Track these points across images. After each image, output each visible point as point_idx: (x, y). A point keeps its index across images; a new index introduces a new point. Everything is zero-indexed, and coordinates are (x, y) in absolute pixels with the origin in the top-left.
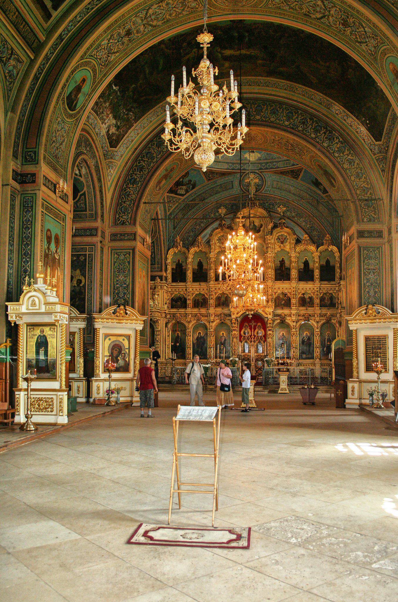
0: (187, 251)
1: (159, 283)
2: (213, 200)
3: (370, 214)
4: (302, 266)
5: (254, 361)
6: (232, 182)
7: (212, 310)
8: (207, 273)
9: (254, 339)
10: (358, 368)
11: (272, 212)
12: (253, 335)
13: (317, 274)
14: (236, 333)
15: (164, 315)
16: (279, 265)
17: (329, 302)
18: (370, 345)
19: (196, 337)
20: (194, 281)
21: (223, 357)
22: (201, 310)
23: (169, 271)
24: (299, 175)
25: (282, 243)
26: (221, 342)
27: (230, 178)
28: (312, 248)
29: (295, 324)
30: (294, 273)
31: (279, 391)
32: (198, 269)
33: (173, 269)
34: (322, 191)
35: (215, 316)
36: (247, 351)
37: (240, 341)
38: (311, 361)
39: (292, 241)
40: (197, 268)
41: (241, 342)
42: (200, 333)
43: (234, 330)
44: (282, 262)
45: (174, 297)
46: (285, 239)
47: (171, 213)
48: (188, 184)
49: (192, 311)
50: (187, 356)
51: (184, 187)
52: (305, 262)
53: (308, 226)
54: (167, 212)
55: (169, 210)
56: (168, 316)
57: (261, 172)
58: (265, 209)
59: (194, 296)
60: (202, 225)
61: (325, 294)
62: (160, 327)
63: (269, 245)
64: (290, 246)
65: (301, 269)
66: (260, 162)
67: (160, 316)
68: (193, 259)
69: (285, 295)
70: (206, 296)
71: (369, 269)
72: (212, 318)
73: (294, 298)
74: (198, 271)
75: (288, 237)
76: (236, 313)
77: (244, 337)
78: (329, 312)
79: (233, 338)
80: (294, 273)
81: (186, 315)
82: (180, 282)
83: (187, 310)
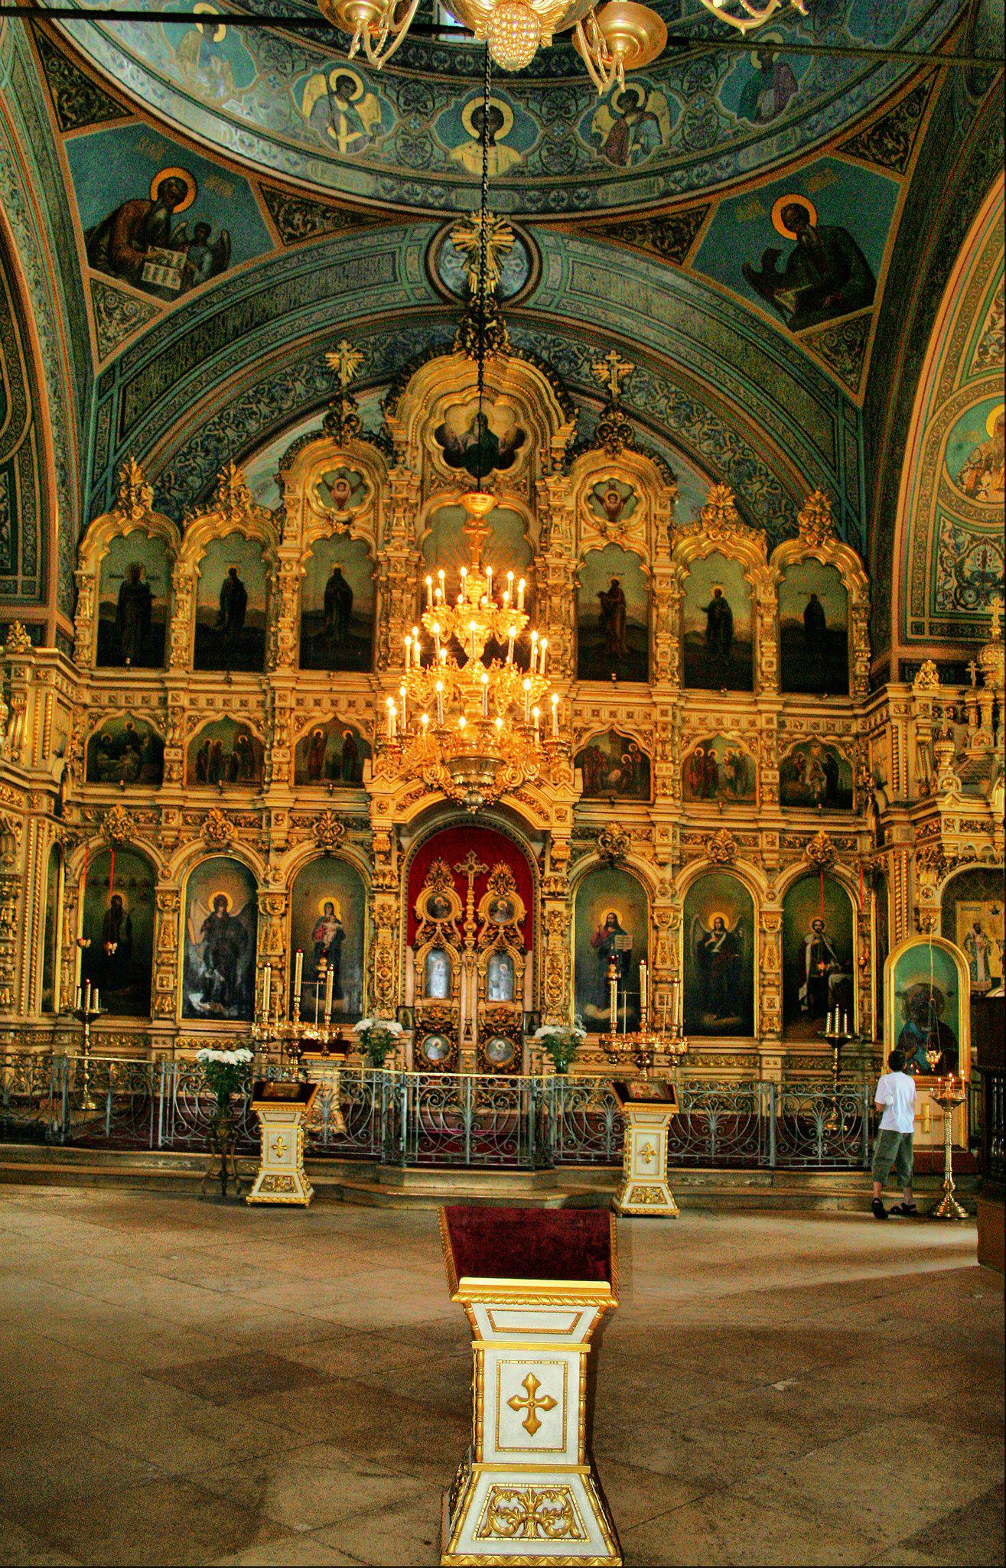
0: (173, 531)
1: (27, 652)
2: (303, 323)
5: (475, 1035)
6: (393, 254)
7: (279, 796)
8: (263, 632)
9: (476, 934)
12: (470, 917)
14: (391, 903)
15: (45, 805)
16: (597, 612)
17: (819, 787)
19: (200, 917)
21: (322, 1014)
22: (228, 796)
23: (89, 609)
24: (691, 242)
25: (613, 515)
26: (320, 945)
27: (388, 240)
28: (750, 545)
29: (667, 874)
30: (666, 650)
32: (221, 614)
33: (104, 607)
34: (789, 316)
35: (295, 823)
36: (438, 990)
37: (412, 942)
38: (739, 1043)
40: (216, 605)
41: (416, 949)
42: (221, 901)
43: (384, 889)
44: (613, 598)
48: (194, 243)
50: (156, 1003)
51: (176, 255)
52: (713, 606)
53: (726, 457)
54: (95, 361)
55: (103, 353)
56: (74, 817)
57: (521, 223)
59: (198, 729)
60: (253, 426)
61: (805, 746)
63: (556, 520)
65: (697, 634)
66: (520, 181)
67: (24, 808)
69: (624, 742)
70: (255, 732)
72: (278, 835)
73: (664, 757)
74: (221, 622)
75: (639, 493)
76: (392, 806)
77: (428, 924)
78: (822, 827)
79: (376, 927)
80: (666, 650)
83: (162, 792)
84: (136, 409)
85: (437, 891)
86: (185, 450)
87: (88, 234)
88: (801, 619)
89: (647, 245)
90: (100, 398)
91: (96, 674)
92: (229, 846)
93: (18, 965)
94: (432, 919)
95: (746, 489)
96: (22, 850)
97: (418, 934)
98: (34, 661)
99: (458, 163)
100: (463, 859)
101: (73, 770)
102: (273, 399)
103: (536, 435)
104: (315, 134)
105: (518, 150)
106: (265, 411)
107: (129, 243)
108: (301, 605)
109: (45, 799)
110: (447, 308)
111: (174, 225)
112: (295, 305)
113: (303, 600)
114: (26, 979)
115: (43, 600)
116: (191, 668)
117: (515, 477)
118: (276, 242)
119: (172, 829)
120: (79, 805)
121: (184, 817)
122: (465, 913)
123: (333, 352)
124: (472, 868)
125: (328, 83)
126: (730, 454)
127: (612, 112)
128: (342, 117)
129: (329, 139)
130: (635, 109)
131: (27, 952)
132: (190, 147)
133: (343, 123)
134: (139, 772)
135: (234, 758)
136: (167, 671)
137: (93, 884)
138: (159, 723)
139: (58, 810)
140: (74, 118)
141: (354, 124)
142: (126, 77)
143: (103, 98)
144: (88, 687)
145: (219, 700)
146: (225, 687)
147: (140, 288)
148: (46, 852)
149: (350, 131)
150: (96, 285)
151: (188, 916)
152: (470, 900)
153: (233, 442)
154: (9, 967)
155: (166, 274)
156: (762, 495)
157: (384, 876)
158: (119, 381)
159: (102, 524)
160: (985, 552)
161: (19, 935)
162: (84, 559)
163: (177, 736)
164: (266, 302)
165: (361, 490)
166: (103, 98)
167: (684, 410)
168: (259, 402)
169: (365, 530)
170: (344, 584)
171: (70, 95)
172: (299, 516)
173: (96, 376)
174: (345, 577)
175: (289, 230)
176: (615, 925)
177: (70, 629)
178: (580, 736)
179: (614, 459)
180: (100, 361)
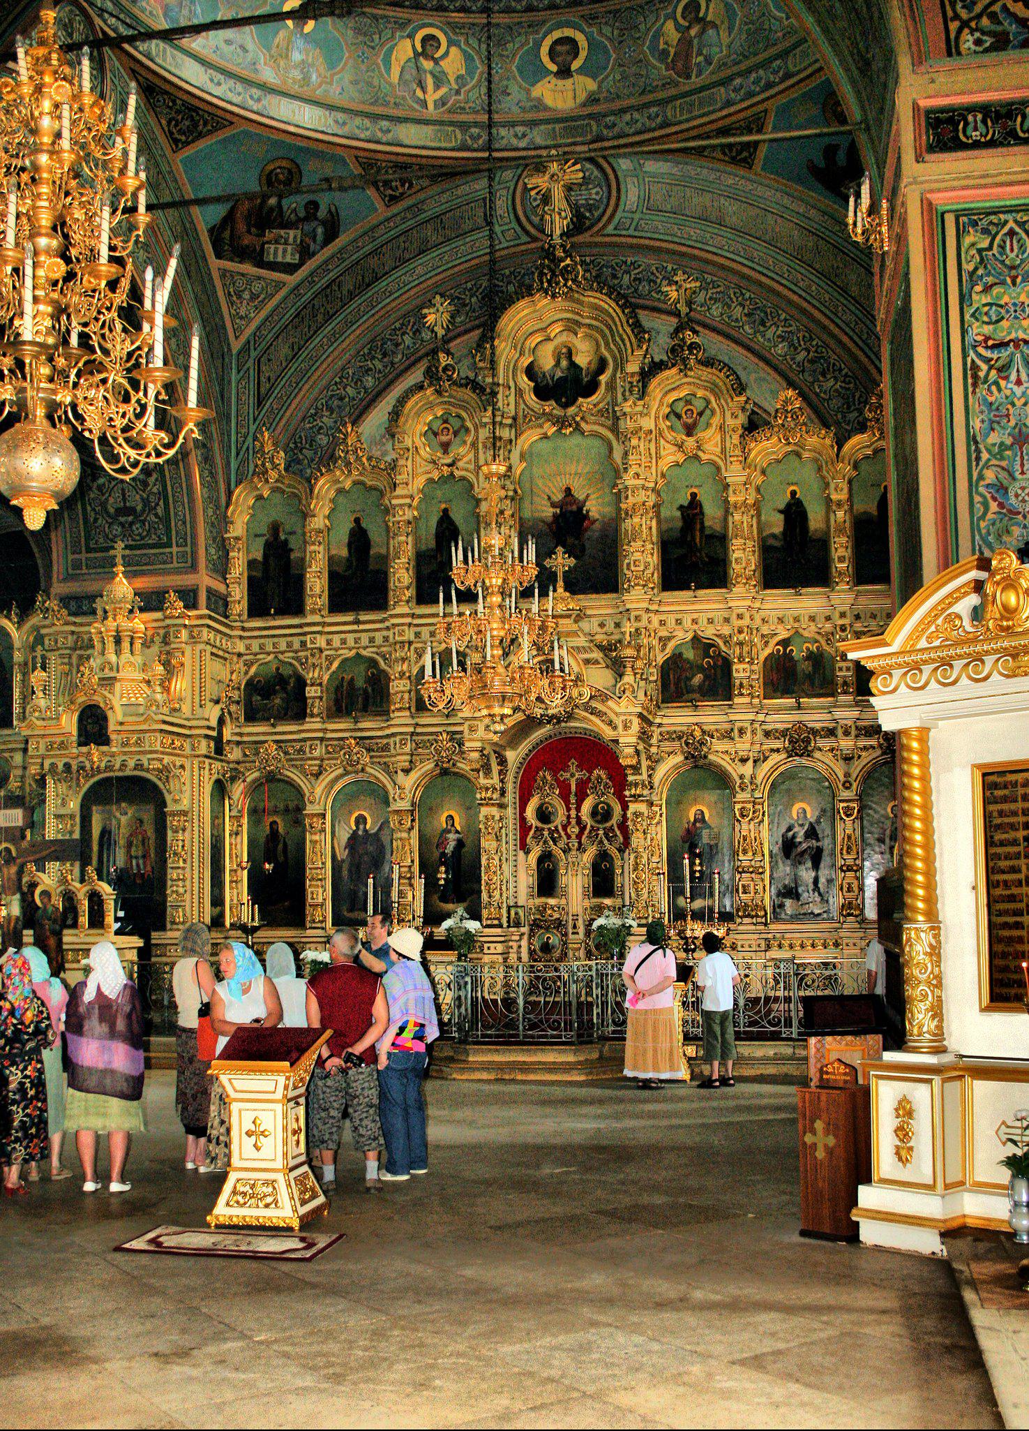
0: (301, 489)
4: (776, 524)
9: (579, 836)
10: (938, 982)
11: (645, 308)
12: (573, 821)
13: (841, 552)
15: (204, 747)
16: (679, 524)
18: (1013, 827)
19: (344, 835)
20: (336, 605)
23: (238, 569)
25: (690, 430)
32: (348, 560)
33: (251, 564)
39: (730, 422)
40: (344, 552)
41: (527, 853)
42: (361, 820)
44: (692, 510)
45: (256, 675)
49: (325, 730)
51: (292, 233)
52: (789, 506)
55: (238, 332)
56: (235, 754)
58: (614, 292)
59: (335, 665)
60: (369, 381)
62: (187, 794)
64: (723, 441)
65: (774, 536)
67: (188, 751)
68: (328, 517)
71: (1003, 345)
74: (349, 567)
82: (276, 613)
84: (269, 379)
85: (543, 797)
86: (312, 411)
87: (211, 231)
91: (247, 625)
92: (363, 770)
93: (188, 887)
94: (540, 825)
97: (528, 840)
98: (187, 622)
99: (539, 100)
100: (565, 768)
101: (230, 713)
102: (385, 355)
103: (614, 358)
104: (404, 98)
105: (594, 77)
106: (379, 366)
107: (249, 232)
108: (415, 544)
109: (204, 742)
110: (533, 245)
111: (285, 208)
113: (417, 540)
114: (196, 900)
115: (194, 568)
116: (326, 612)
117: (598, 403)
118: (379, 205)
119: (315, 759)
120: (238, 743)
121: (327, 746)
122: (569, 817)
123: (428, 307)
124: (573, 774)
125: (413, 46)
126: (804, 354)
127: (678, 27)
128: (429, 76)
131: (196, 876)
132: (288, 139)
133: (430, 82)
134: (286, 709)
135: (365, 691)
136: (305, 616)
137: (254, 812)
138: (302, 664)
139: (219, 750)
140: (183, 138)
142: (221, 92)
143: (206, 116)
144: (241, 637)
145: (350, 638)
146: (355, 627)
147: (262, 268)
148: (208, 788)
149: (437, 87)
153: (354, 399)
154: (181, 890)
155: (285, 251)
156: (836, 391)
157: (487, 789)
158: (253, 354)
159: (241, 493)
160: (123, 490)
161: (189, 862)
162: (232, 523)
163: (316, 675)
165: (463, 431)
166: (206, 116)
169: (467, 470)
170: (452, 522)
171: (177, 121)
172: (409, 463)
173: (234, 352)
174: (451, 515)
176: (703, 820)
177: (222, 588)
178: (665, 645)
179: (686, 376)
180: (237, 338)
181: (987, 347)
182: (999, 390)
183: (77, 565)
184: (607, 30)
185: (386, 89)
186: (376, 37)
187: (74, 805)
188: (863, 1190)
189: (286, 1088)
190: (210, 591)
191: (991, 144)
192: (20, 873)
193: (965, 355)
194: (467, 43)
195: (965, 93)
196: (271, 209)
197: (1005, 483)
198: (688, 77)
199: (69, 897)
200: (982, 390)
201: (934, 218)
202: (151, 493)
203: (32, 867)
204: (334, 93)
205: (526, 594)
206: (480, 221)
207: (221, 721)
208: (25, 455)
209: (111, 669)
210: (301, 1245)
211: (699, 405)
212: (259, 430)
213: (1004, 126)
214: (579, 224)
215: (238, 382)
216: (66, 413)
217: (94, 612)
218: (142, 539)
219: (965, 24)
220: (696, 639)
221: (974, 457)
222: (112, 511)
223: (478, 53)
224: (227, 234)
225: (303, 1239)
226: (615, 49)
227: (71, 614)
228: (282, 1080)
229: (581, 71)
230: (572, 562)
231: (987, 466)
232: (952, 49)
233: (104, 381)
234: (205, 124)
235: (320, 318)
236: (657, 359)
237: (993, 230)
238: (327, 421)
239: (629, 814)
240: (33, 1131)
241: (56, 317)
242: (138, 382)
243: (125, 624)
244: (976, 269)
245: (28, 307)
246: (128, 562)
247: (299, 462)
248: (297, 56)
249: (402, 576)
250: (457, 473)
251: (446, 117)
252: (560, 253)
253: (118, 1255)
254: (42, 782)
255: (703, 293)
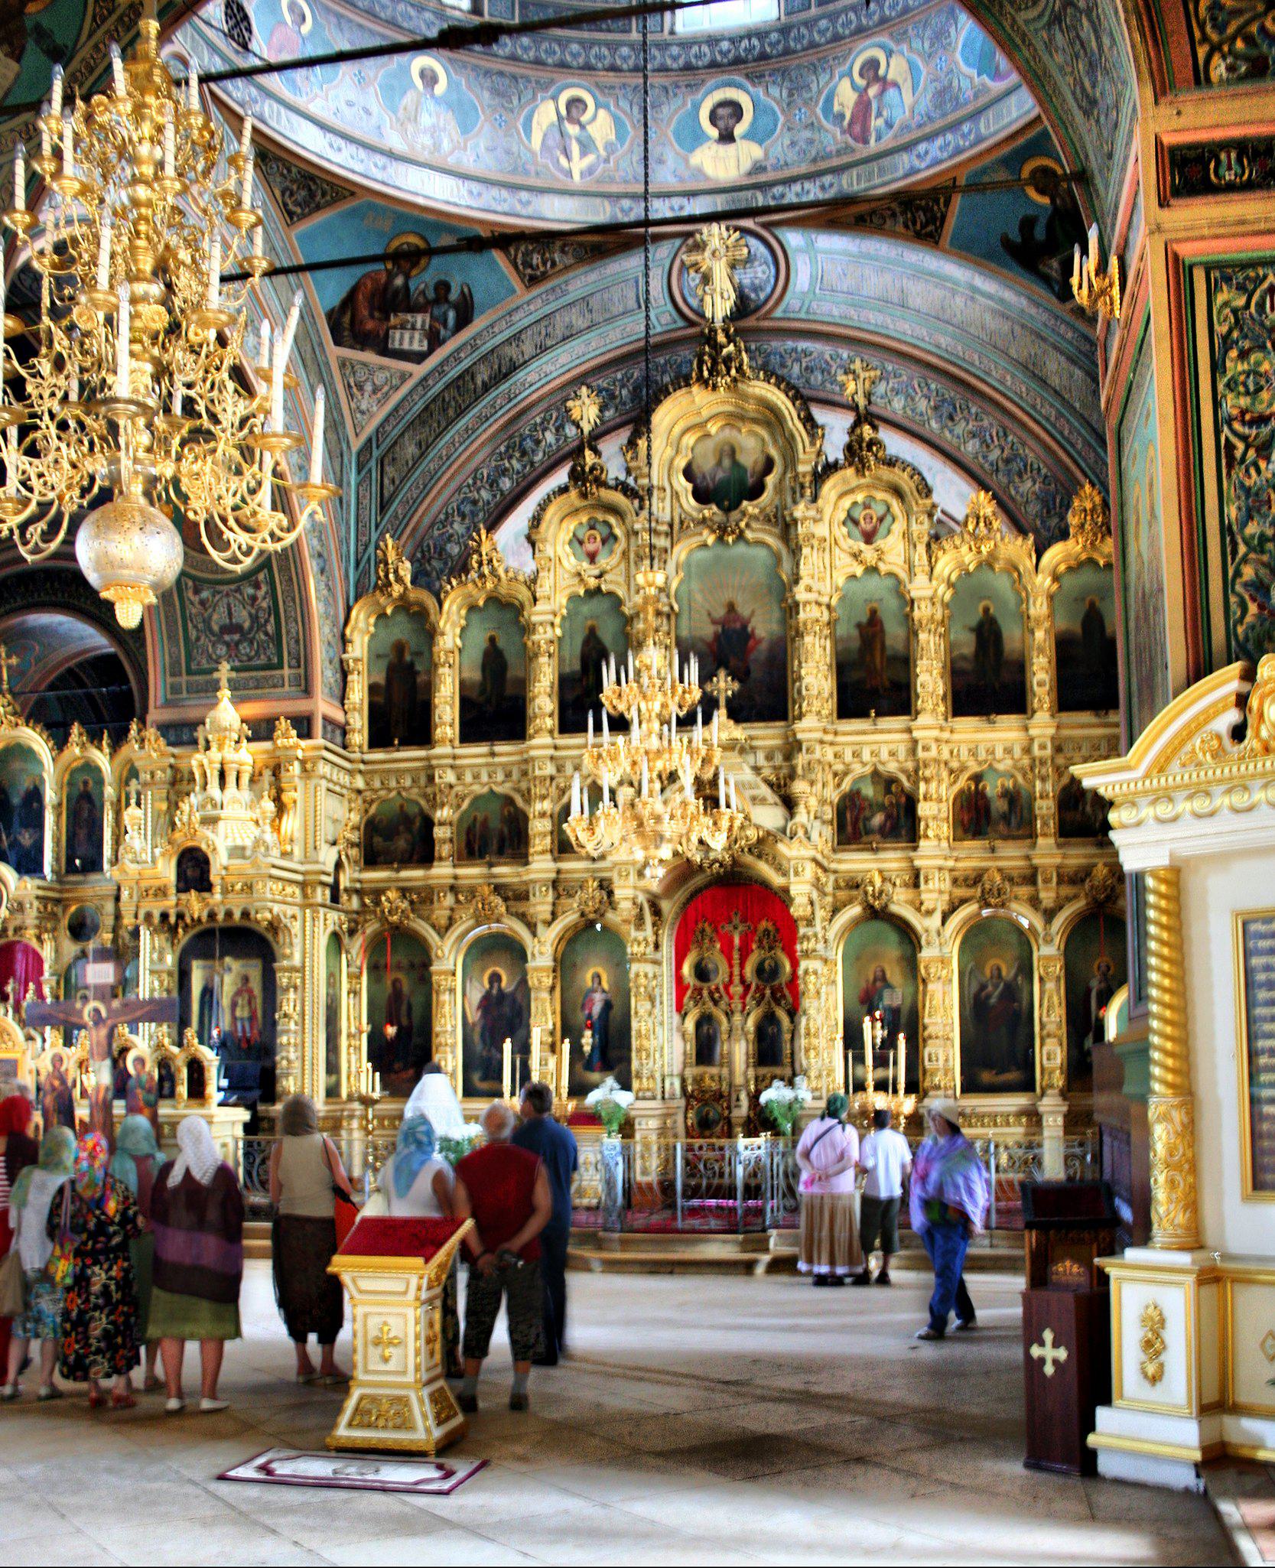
0: (430, 602)
3: (1254, 28)
4: (967, 644)
12: (736, 979)
15: (322, 895)
16: (856, 644)
19: (476, 995)
23: (358, 693)
24: (943, 218)
25: (869, 538)
28: (1016, 548)
31: (343, 1432)
33: (373, 689)
38: (1014, 1102)
42: (495, 978)
46: (881, 520)
47: (370, 440)
48: (437, 301)
59: (465, 805)
65: (963, 657)
66: (762, 178)
67: (299, 899)
69: (888, 783)
81: (422, 899)
84: (393, 481)
88: (1077, 628)
89: (900, 229)
90: (359, 472)
94: (699, 984)
95: (1016, 489)
96: (297, 941)
97: (686, 999)
104: (546, 166)
105: (760, 143)
106: (517, 465)
112: (543, 349)
115: (307, 691)
116: (457, 742)
122: (731, 975)
127: (854, 86)
129: (561, 170)
130: (877, 78)
133: (575, 149)
135: (501, 833)
139: (335, 898)
141: (586, 146)
146: (490, 760)
148: (323, 940)
149: (584, 154)
150: (343, 364)
151: (464, 994)
152: (736, 961)
155: (412, 338)
158: (376, 453)
164: (511, 351)
167: (946, 409)
168: (510, 457)
170: (599, 642)
173: (355, 449)
175: (529, 271)
176: (884, 978)
177: (339, 716)
181: (1243, 423)
182: (1258, 471)
183: (175, 689)
184: (774, 91)
185: (526, 156)
186: (515, 101)
187: (170, 960)
188: (1102, 1414)
189: (419, 1289)
190: (326, 719)
191: (1248, 187)
192: (111, 1036)
193: (1217, 432)
194: (617, 105)
195: (1217, 126)
196: (397, 291)
197: (1266, 580)
198: (866, 142)
199: (164, 1064)
200: (1239, 473)
201: (1180, 271)
202: (260, 608)
203: (124, 1030)
204: (468, 162)
205: (686, 722)
206: (632, 304)
207: (339, 865)
208: (117, 537)
209: (215, 806)
210: (437, 1474)
211: (878, 510)
212: (381, 537)
213: (1263, 166)
214: (744, 307)
215: (358, 485)
216: (167, 490)
217: (194, 742)
218: (250, 659)
219: (1215, 48)
220: (876, 774)
221: (1229, 547)
222: (216, 628)
223: (630, 116)
224: (347, 319)
225: (440, 1467)
226: (783, 111)
227: (170, 744)
228: (414, 1282)
229: (746, 137)
230: (736, 686)
231: (1245, 560)
232: (1200, 78)
233: (214, 451)
234: (324, 194)
235: (451, 412)
236: (831, 459)
237: (1251, 287)
238: (458, 527)
239: (801, 972)
240: (119, 1340)
241: (157, 378)
242: (251, 451)
243: (229, 753)
244: (1230, 331)
245: (124, 362)
246: (234, 686)
247: (427, 574)
248: (426, 120)
249: (544, 702)
250: (604, 588)
251: (594, 188)
252: (721, 338)
253: (223, 1488)
254: (135, 934)
255: (883, 384)
